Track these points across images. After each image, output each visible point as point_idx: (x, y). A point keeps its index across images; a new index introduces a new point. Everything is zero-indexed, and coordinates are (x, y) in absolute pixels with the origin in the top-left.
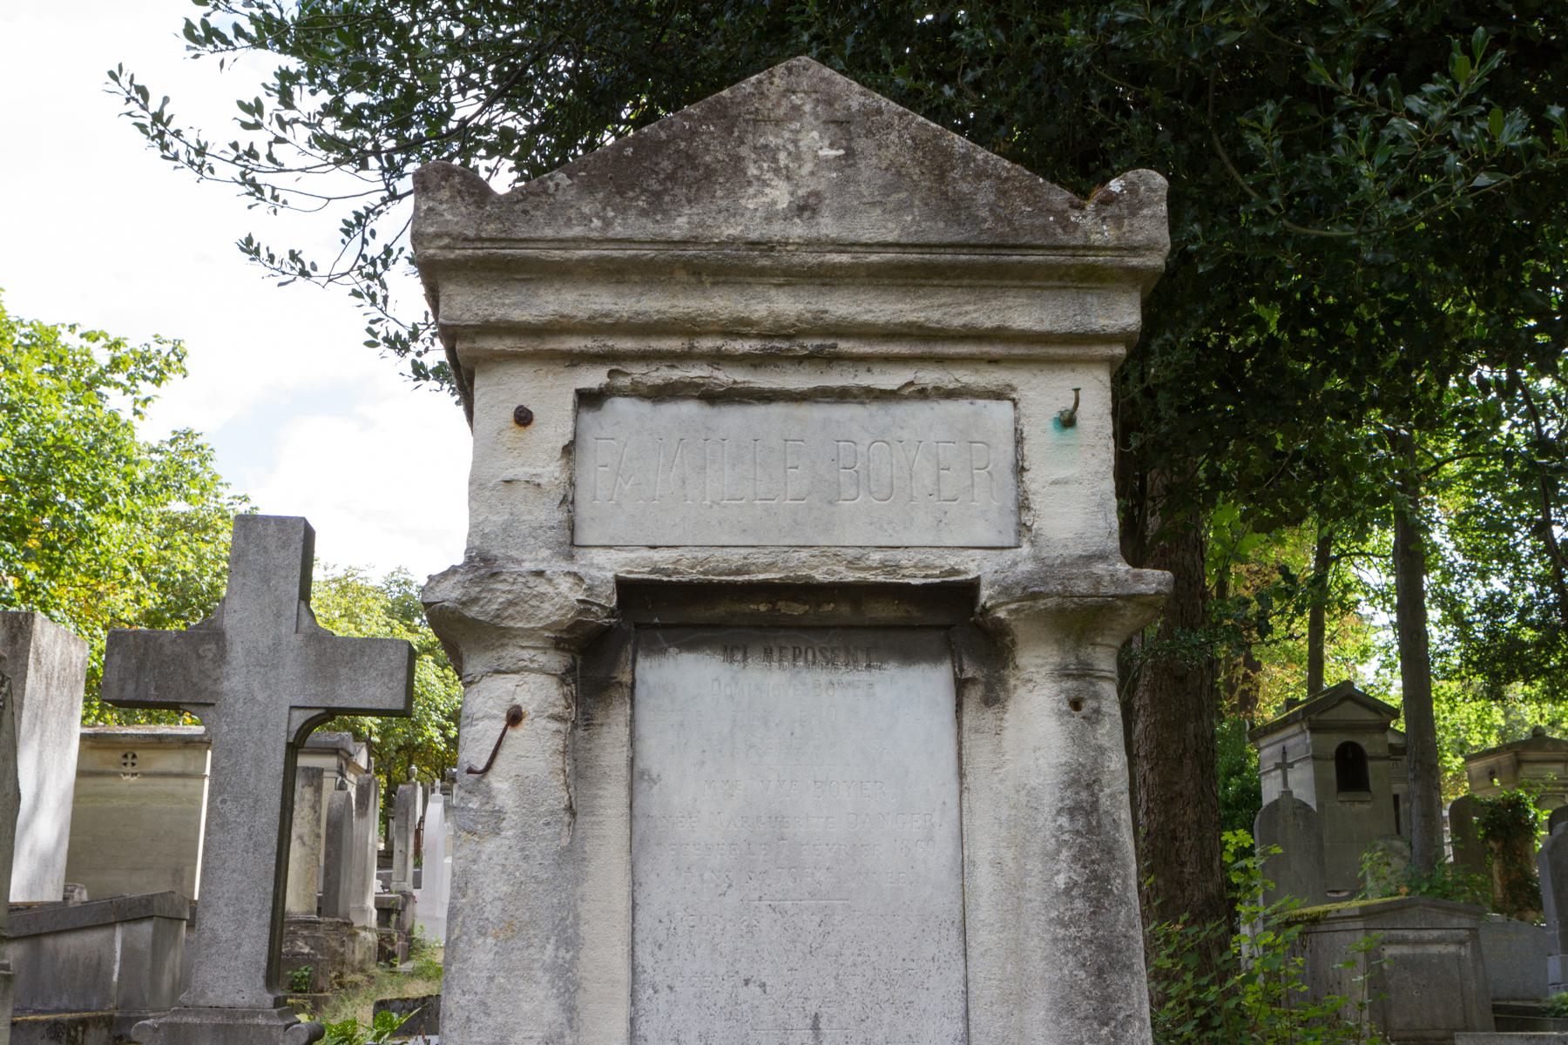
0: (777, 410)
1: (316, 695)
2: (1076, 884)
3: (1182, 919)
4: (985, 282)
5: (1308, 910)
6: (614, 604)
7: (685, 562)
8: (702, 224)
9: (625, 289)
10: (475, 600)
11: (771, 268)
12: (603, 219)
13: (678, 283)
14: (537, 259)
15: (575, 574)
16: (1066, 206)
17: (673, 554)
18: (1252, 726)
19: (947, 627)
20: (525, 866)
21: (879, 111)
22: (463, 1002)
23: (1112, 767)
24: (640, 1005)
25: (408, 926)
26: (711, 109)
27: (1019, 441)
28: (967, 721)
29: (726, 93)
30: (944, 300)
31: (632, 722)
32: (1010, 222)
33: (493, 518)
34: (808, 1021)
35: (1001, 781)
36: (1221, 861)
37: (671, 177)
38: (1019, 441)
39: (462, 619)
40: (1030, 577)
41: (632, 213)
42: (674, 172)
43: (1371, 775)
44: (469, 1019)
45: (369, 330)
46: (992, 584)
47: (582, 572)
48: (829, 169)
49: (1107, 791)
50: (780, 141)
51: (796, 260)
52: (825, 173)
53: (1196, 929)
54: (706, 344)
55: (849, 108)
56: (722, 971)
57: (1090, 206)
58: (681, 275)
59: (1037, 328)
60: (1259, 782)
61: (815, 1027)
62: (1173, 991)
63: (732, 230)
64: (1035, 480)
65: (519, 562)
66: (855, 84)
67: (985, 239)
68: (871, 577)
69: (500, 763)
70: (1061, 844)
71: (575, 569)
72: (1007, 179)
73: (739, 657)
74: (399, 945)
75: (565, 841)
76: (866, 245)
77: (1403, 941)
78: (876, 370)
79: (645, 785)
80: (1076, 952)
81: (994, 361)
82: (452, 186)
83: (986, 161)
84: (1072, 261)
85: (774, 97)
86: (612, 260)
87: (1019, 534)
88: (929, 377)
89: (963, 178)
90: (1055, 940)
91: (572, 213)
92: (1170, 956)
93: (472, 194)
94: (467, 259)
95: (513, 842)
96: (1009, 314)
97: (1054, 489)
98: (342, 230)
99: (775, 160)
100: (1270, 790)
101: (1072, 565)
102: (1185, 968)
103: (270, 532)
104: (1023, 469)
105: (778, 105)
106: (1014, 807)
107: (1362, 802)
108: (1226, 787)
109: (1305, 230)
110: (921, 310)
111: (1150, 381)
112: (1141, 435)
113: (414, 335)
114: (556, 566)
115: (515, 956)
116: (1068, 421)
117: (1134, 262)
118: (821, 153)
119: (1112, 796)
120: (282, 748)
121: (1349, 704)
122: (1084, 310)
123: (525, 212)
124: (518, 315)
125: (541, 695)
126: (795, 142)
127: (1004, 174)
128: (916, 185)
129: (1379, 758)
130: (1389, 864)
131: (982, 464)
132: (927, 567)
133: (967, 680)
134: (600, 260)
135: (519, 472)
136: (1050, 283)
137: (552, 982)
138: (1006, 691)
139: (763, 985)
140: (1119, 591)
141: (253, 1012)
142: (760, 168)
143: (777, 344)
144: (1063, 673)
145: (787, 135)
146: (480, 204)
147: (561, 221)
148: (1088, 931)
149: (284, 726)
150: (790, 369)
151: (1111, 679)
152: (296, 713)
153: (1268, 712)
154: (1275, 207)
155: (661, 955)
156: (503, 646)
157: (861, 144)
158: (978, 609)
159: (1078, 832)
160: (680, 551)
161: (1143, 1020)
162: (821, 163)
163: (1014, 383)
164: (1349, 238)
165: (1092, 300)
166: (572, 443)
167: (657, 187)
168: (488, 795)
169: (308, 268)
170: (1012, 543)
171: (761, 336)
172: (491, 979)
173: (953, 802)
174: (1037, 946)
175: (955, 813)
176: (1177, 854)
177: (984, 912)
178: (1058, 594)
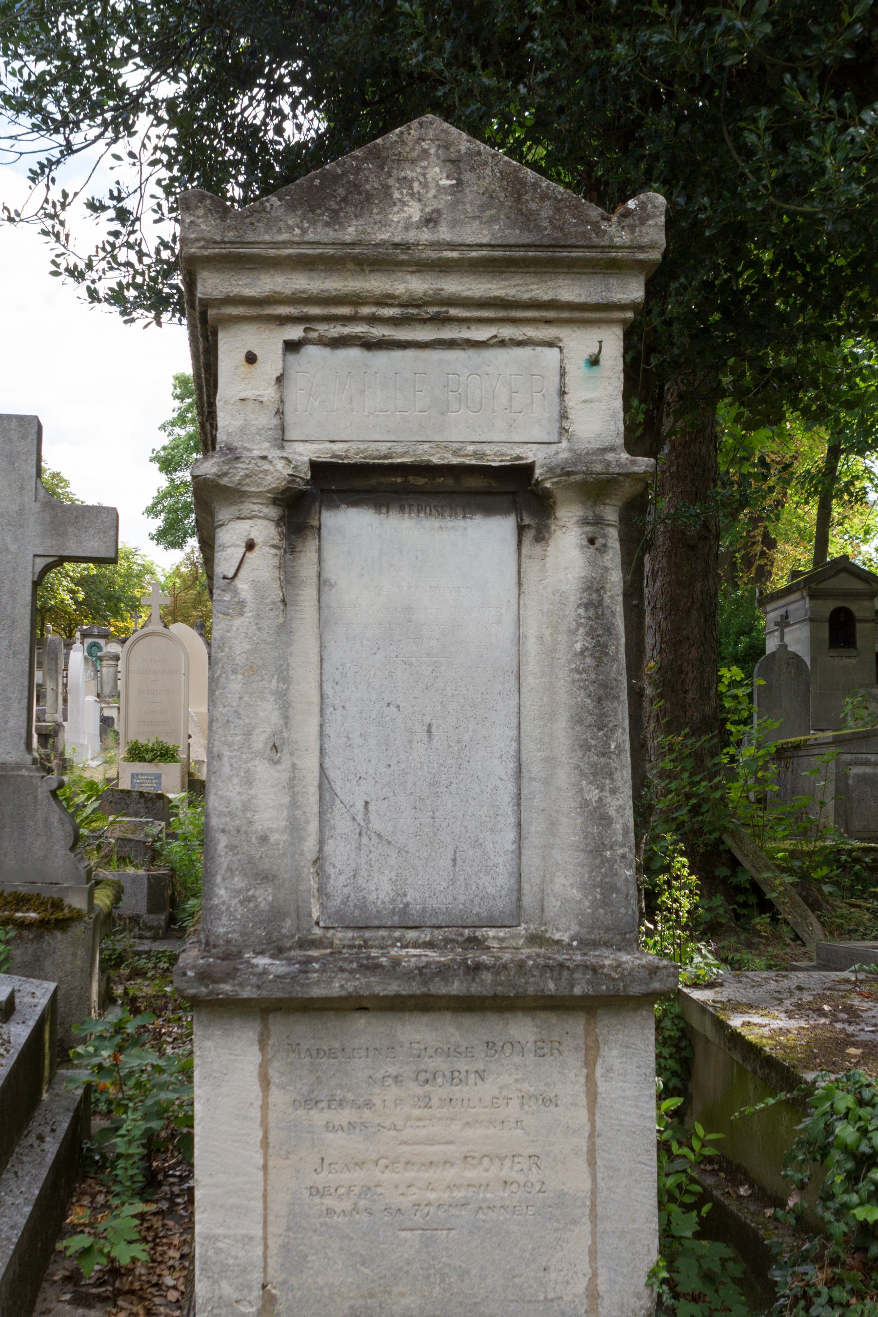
0: (410, 353)
1: (52, 547)
2: (587, 648)
3: (683, 733)
4: (545, 270)
5: (793, 740)
6: (309, 477)
7: (352, 451)
8: (364, 232)
9: (314, 275)
10: (225, 474)
11: (408, 261)
12: (302, 228)
13: (349, 270)
14: (260, 256)
15: (286, 458)
16: (599, 218)
17: (345, 446)
18: (761, 593)
19: (514, 493)
20: (259, 634)
21: (479, 153)
22: (224, 711)
23: (613, 579)
24: (326, 717)
25: (60, 749)
26: (370, 152)
27: (563, 374)
28: (524, 551)
29: (379, 141)
30: (517, 282)
31: (319, 550)
32: (562, 229)
33: (233, 423)
34: (425, 728)
35: (544, 588)
36: (717, 690)
37: (344, 200)
38: (563, 374)
39: (218, 486)
40: (566, 462)
41: (319, 224)
42: (346, 196)
43: (858, 635)
44: (228, 721)
45: (54, 262)
46: (542, 466)
47: (290, 457)
48: (446, 194)
49: (609, 594)
50: (414, 174)
51: (424, 256)
52: (443, 196)
53: (694, 739)
54: (366, 311)
55: (459, 151)
56: (374, 698)
57: (614, 219)
58: (351, 266)
59: (577, 300)
60: (764, 640)
61: (429, 731)
62: (673, 786)
63: (384, 236)
64: (571, 400)
65: (250, 450)
66: (464, 134)
67: (545, 241)
68: (467, 461)
69: (242, 572)
70: (579, 625)
71: (285, 455)
72: (561, 200)
73: (384, 510)
74: (54, 763)
75: (281, 620)
76: (469, 245)
77: (867, 763)
78: (473, 327)
79: (327, 588)
80: (586, 688)
81: (548, 322)
82: (205, 207)
83: (548, 188)
84: (600, 256)
85: (411, 144)
86: (307, 256)
87: (560, 434)
88: (507, 332)
89: (532, 200)
90: (573, 681)
91: (282, 224)
92: (672, 761)
93: (218, 212)
94: (216, 255)
95: (252, 620)
96: (559, 291)
97: (584, 405)
98: (29, 178)
99: (411, 188)
100: (772, 645)
101: (593, 454)
102: (683, 769)
103: (13, 427)
104: (565, 393)
105: (413, 149)
106: (552, 604)
107: (849, 657)
108: (736, 644)
109: (787, 206)
110: (502, 288)
111: (668, 316)
112: (659, 356)
113: (90, 266)
114: (274, 454)
115: (255, 685)
116: (594, 361)
117: (641, 256)
118: (441, 182)
119: (612, 597)
120: (29, 585)
121: (843, 575)
122: (608, 289)
123: (252, 224)
124: (247, 292)
125: (266, 532)
126: (424, 175)
127: (559, 197)
128: (502, 204)
129: (866, 621)
130: (866, 708)
131: (539, 389)
132: (502, 455)
133: (525, 526)
134: (300, 256)
135: (249, 393)
136: (587, 270)
137: (275, 701)
138: (549, 533)
139: (398, 707)
140: (621, 471)
141: (18, 767)
142: (402, 193)
143: (412, 311)
144: (585, 522)
145: (419, 170)
146: (223, 219)
147: (275, 230)
148: (593, 676)
149: (30, 569)
150: (419, 327)
151: (615, 526)
152: (38, 560)
153: (780, 581)
154: (765, 186)
155: (337, 688)
156: (242, 502)
157: (467, 176)
158: (533, 482)
159: (590, 618)
160: (349, 444)
161: (624, 729)
162: (440, 189)
163: (561, 336)
164: (817, 213)
165: (613, 281)
166: (282, 375)
167: (335, 207)
168: (236, 592)
169: (13, 215)
170: (556, 439)
171: (400, 305)
172: (241, 698)
173: (514, 601)
174: (562, 685)
175: (515, 607)
176: (683, 685)
177: (531, 666)
178: (583, 473)
